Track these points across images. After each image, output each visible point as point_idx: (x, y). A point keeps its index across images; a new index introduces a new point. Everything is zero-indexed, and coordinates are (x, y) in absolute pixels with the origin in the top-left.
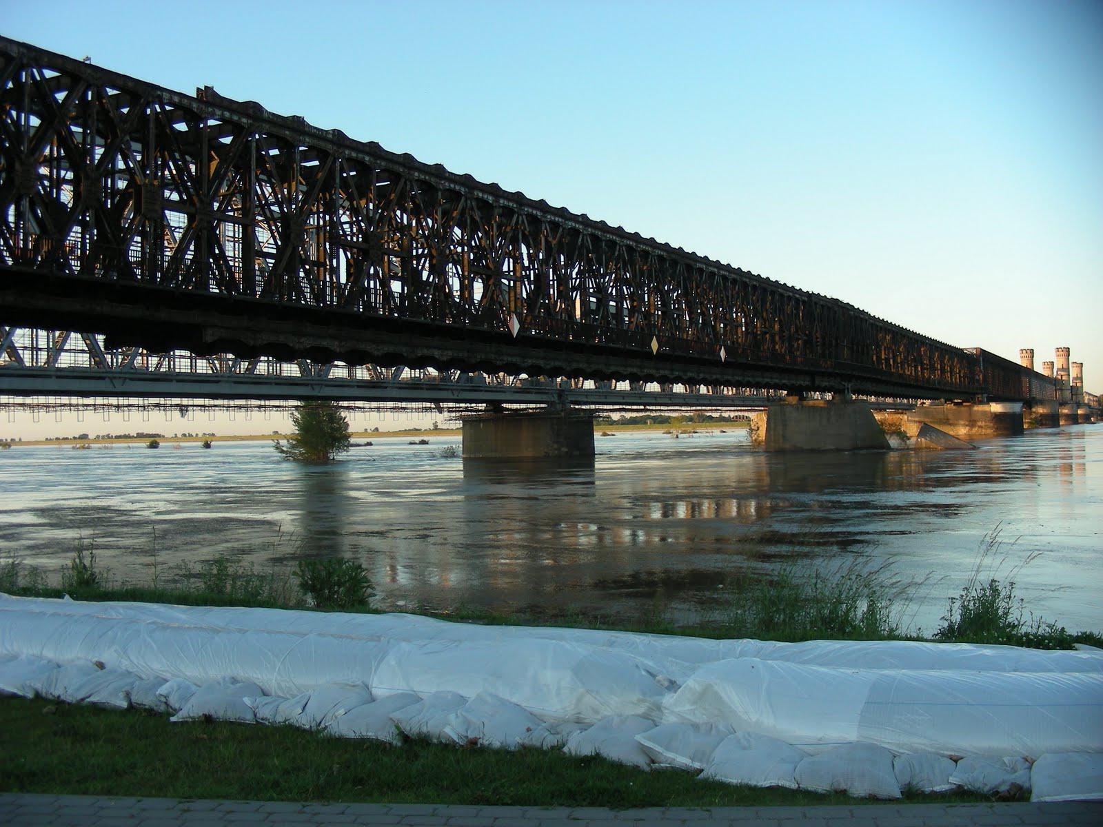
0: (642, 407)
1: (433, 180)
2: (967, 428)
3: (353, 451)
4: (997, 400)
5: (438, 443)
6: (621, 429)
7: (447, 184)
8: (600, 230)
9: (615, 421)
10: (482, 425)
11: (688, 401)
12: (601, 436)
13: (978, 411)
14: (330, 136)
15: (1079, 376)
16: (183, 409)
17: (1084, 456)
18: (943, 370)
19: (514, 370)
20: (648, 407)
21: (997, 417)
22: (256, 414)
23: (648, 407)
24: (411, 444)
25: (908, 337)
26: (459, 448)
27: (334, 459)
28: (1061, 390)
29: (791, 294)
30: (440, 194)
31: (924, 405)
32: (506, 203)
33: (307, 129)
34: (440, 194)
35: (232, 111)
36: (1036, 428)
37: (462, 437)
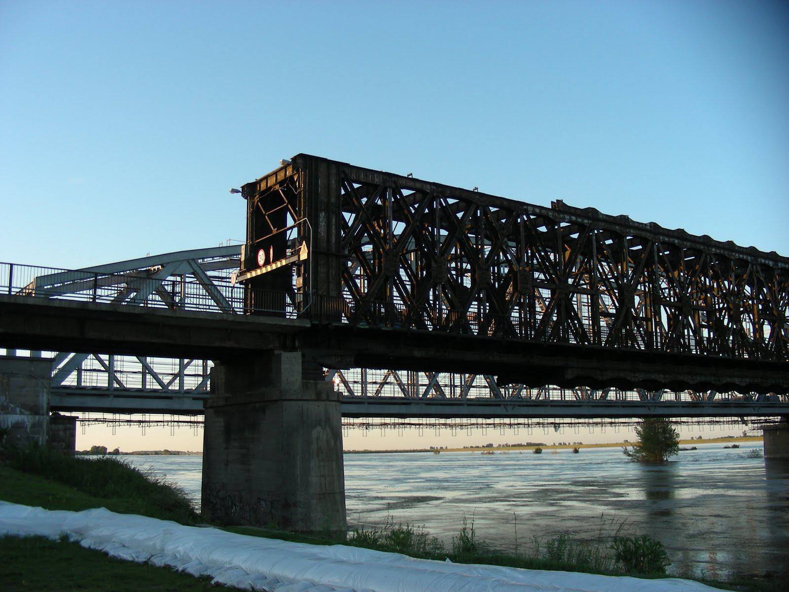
1: (726, 253)
10: (778, 433)
16: (556, 426)
22: (609, 429)
24: (726, 448)
27: (667, 460)
30: (732, 263)
35: (577, 216)
37: (763, 442)
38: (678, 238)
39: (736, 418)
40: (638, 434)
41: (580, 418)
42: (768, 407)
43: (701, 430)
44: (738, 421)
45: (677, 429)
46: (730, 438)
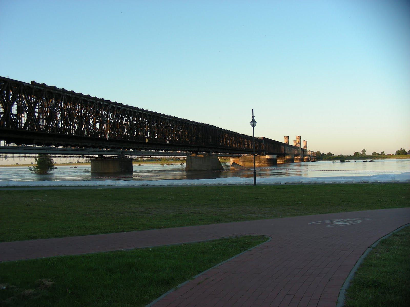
0: (149, 156)
1: (87, 99)
2: (259, 163)
3: (55, 170)
4: (266, 154)
5: (81, 168)
6: (147, 163)
7: (90, 100)
8: (132, 109)
9: (145, 160)
10: (97, 162)
11: (164, 154)
12: (139, 165)
13: (262, 158)
14: (62, 90)
15: (306, 145)
16: (6, 157)
17: (301, 175)
18: (248, 145)
19: (107, 148)
20: (151, 156)
21: (268, 159)
22: (28, 159)
23: (151, 156)
24: (71, 168)
25: (234, 134)
26: (90, 170)
27: (49, 173)
28: (298, 150)
29: (192, 123)
30: (88, 103)
31: (245, 156)
32: (106, 103)
33: (56, 89)
34: (88, 103)
35: (39, 86)
36: (286, 163)
37: (90, 166)
38: (71, 94)
39: (80, 156)
40: (36, 161)
41: (16, 154)
42: (94, 151)
43: (57, 160)
44: (81, 156)
45: (55, 160)
46: (71, 163)
